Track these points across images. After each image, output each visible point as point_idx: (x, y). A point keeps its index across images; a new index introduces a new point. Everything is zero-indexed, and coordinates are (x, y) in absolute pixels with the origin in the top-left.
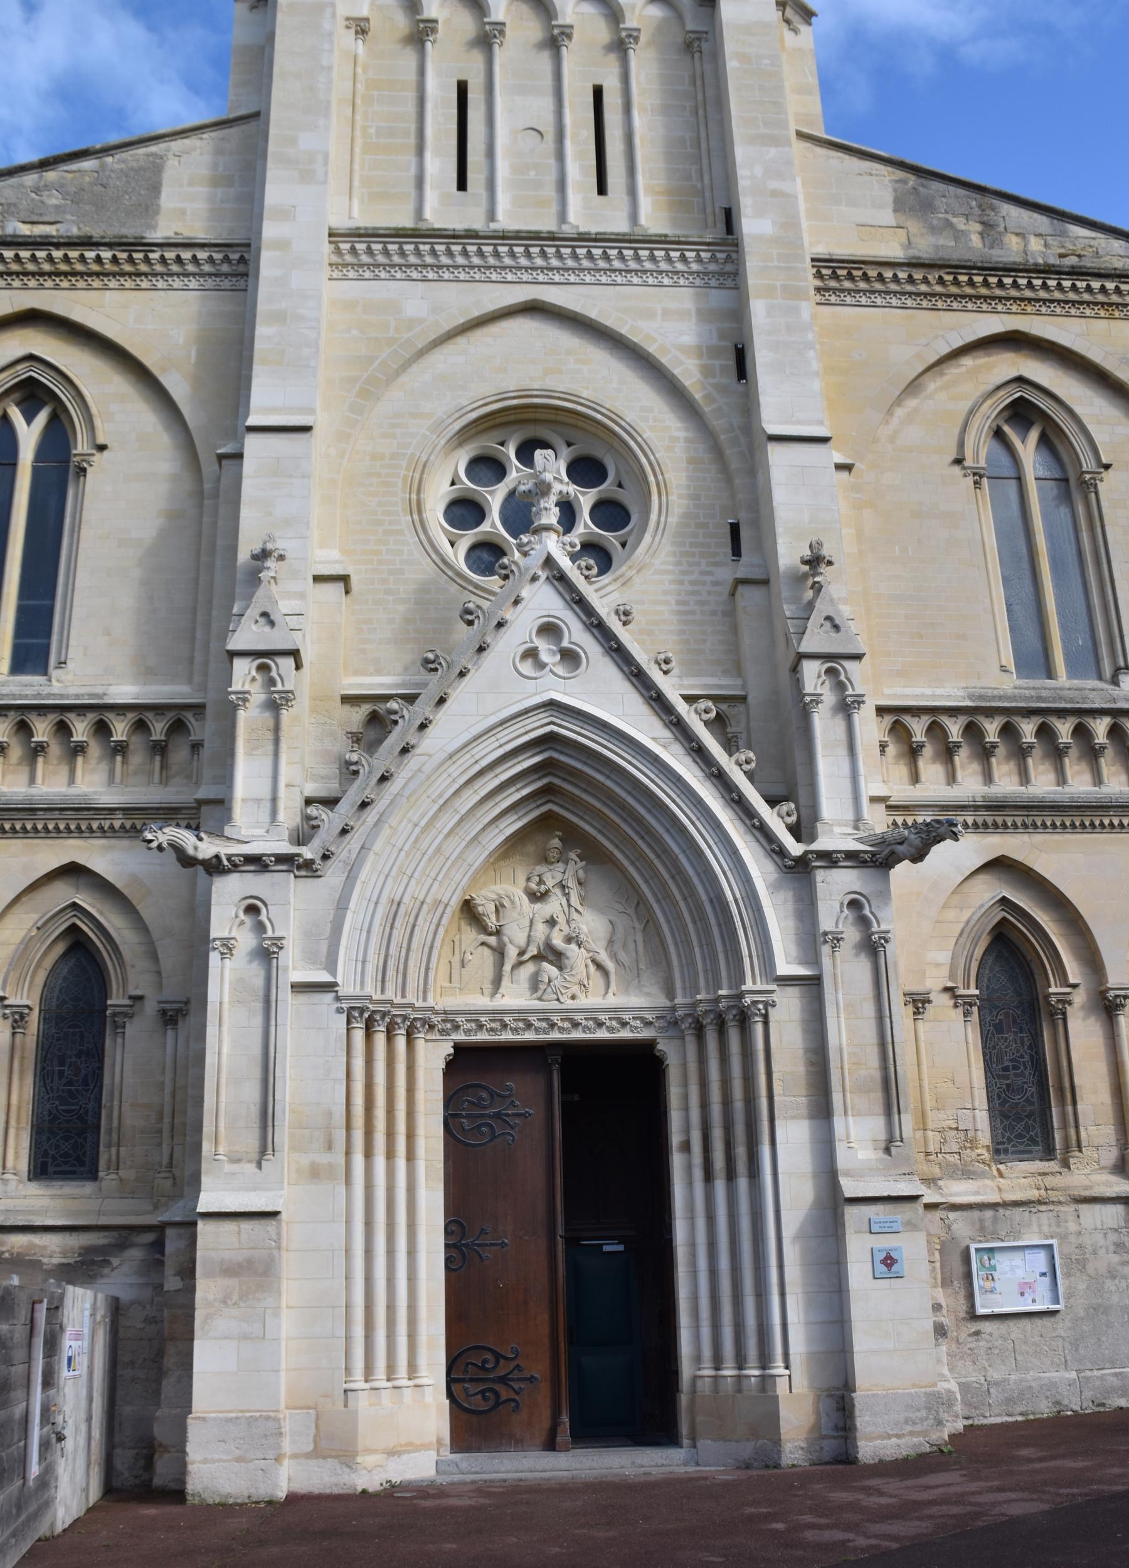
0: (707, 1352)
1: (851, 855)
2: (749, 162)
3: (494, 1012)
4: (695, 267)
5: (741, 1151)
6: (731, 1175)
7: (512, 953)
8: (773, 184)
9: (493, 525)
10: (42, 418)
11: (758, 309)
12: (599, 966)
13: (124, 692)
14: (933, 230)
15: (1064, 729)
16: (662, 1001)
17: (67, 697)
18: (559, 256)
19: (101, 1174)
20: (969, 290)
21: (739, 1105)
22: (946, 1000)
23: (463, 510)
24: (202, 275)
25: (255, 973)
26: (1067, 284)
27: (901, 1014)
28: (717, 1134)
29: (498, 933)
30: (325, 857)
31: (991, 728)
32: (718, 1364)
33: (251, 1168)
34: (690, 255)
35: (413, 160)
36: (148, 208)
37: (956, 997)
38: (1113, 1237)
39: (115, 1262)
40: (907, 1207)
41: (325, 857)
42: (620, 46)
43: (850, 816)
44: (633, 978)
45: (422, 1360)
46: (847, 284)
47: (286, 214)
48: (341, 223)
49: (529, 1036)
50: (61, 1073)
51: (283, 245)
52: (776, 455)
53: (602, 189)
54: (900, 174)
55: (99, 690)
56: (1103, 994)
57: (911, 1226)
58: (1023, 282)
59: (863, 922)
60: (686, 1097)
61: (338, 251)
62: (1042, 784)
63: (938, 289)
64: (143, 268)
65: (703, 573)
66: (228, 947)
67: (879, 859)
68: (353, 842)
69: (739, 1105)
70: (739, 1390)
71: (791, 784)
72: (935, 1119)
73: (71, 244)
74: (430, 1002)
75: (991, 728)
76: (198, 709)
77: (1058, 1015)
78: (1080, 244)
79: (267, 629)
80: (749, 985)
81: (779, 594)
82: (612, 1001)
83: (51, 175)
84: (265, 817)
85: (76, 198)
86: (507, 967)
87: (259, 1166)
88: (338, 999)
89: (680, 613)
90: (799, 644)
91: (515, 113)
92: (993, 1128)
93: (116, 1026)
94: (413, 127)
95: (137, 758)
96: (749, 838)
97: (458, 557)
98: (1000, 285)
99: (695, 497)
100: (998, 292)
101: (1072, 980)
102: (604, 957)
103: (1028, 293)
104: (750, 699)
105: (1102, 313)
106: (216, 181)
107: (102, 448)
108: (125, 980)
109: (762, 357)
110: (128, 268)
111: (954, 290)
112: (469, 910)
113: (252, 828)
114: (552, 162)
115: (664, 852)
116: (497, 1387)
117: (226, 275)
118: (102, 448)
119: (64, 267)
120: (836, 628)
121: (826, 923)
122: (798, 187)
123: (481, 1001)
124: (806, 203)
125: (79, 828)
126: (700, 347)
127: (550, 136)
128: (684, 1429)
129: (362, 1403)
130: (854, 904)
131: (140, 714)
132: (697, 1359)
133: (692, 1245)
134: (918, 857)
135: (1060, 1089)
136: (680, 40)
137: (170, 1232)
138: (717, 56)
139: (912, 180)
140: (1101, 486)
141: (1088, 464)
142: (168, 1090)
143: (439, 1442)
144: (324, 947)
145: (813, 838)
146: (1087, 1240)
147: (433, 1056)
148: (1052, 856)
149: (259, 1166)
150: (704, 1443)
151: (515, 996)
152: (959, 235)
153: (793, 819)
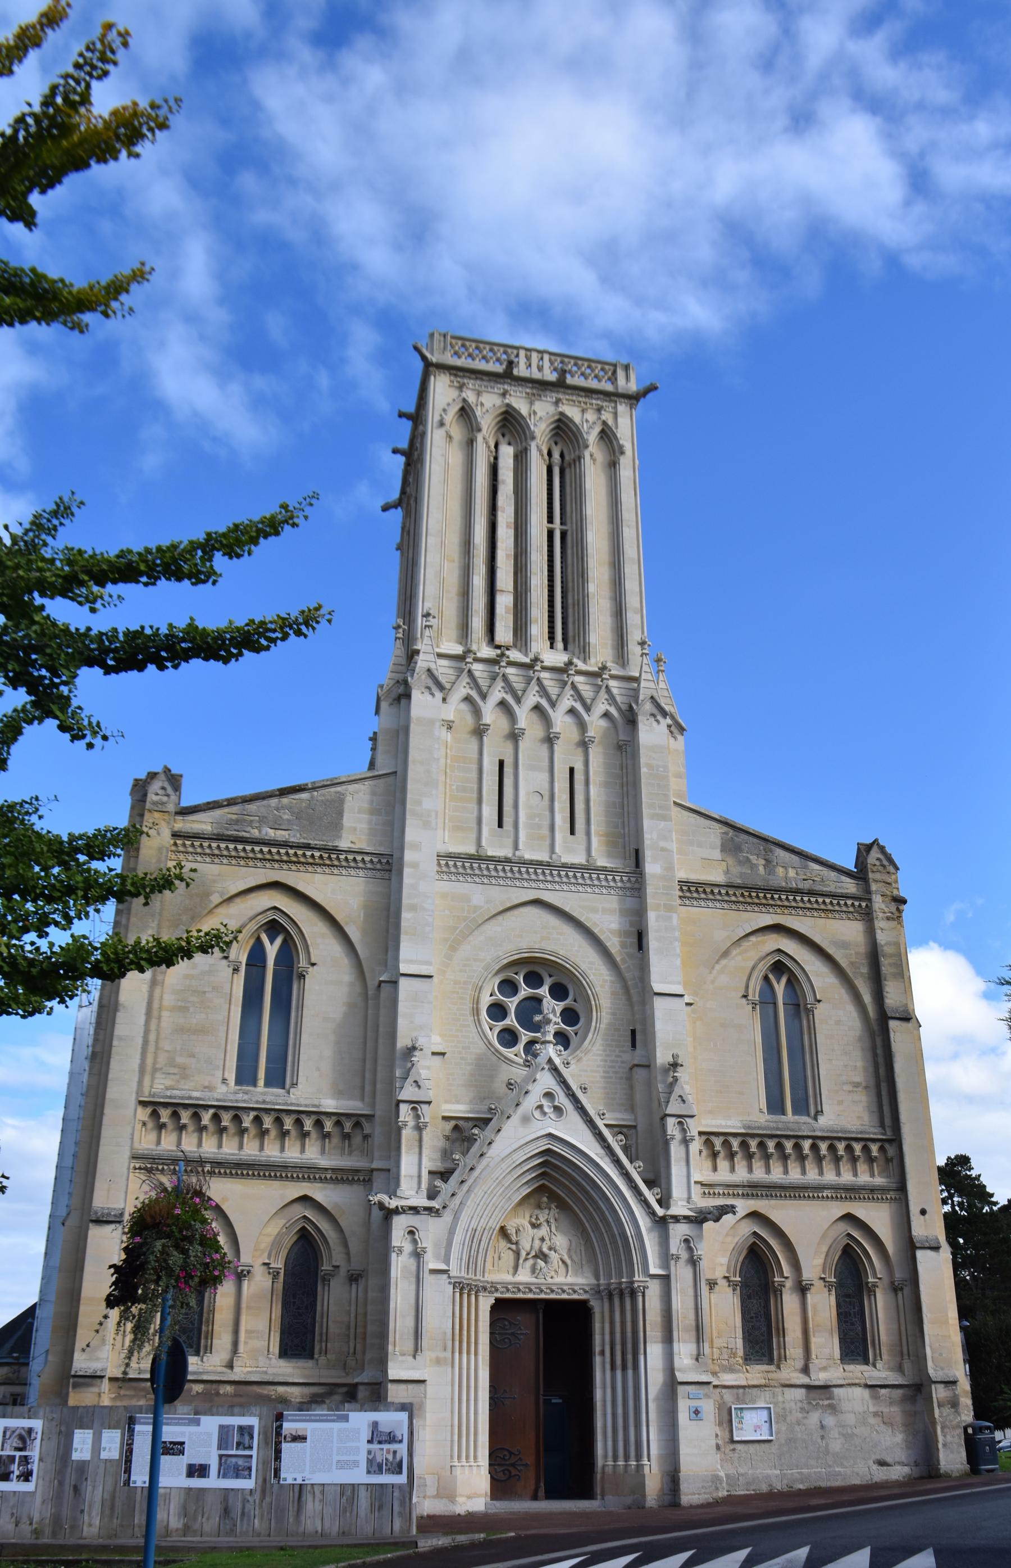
0: (610, 1454)
1: (686, 1217)
2: (652, 831)
3: (515, 1283)
4: (619, 884)
5: (630, 1357)
6: (624, 1368)
7: (523, 1254)
8: (662, 844)
9: (512, 1021)
10: (279, 941)
11: (652, 916)
12: (563, 1262)
13: (330, 1104)
14: (740, 863)
15: (789, 1145)
16: (593, 1281)
17: (301, 1106)
18: (551, 875)
19: (316, 1356)
20: (756, 901)
21: (629, 1335)
22: (725, 1283)
23: (498, 1011)
24: (366, 869)
25: (412, 1263)
26: (806, 899)
27: (704, 1288)
28: (618, 1348)
29: (517, 1243)
30: (444, 1207)
31: (753, 1144)
32: (615, 1458)
33: (411, 1358)
34: (618, 878)
35: (475, 807)
36: (336, 826)
37: (729, 1281)
38: (799, 1405)
39: (327, 1401)
40: (705, 1387)
41: (444, 1207)
42: (584, 744)
43: (685, 1196)
44: (579, 1268)
45: (479, 1454)
46: (695, 895)
47: (417, 847)
48: (444, 849)
49: (530, 1296)
50: (294, 1303)
51: (415, 865)
52: (658, 1002)
53: (572, 832)
54: (725, 829)
55: (316, 1102)
56: (800, 1282)
57: (707, 1396)
58: (784, 897)
59: (690, 1249)
60: (603, 1329)
61: (439, 865)
62: (776, 1175)
63: (741, 899)
64: (336, 863)
65: (617, 1056)
66: (400, 1250)
67: (699, 1219)
68: (457, 1200)
69: (629, 1335)
70: (626, 1471)
71: (657, 1178)
72: (718, 1342)
73: (299, 846)
74: (486, 1279)
75: (753, 1144)
76: (370, 1117)
77: (778, 1292)
78: (814, 873)
79: (417, 1089)
80: (636, 1278)
81: (656, 1077)
82: (570, 1279)
83: (285, 800)
84: (415, 1186)
85: (298, 816)
86: (521, 1261)
87: (414, 1357)
88: (449, 1277)
89: (605, 1077)
90: (667, 1106)
91: (530, 781)
92: (744, 1347)
93: (324, 1280)
94: (475, 786)
95: (336, 1140)
96: (639, 1206)
97: (493, 1037)
98: (772, 898)
99: (614, 1014)
100: (771, 902)
101: (786, 1275)
102: (566, 1258)
103: (786, 903)
104: (639, 1128)
105: (823, 915)
106: (373, 812)
107: (313, 965)
108: (331, 1257)
109: (653, 943)
110: (328, 862)
111: (749, 900)
112: (503, 1231)
113: (411, 1191)
114: (547, 813)
115: (598, 1208)
116: (510, 1468)
117: (379, 870)
118: (313, 965)
119: (294, 859)
120: (684, 1101)
121: (673, 1250)
122: (674, 847)
123: (508, 1278)
124: (679, 851)
125: (309, 1177)
126: (620, 931)
127: (546, 798)
128: (598, 1490)
129: (458, 1472)
130: (686, 1241)
131: (339, 1119)
132: (605, 1456)
133: (604, 1401)
134: (717, 1220)
135: (778, 1329)
136: (615, 742)
137: (361, 1388)
138: (635, 755)
139: (731, 833)
140: (815, 1011)
141: (810, 999)
142: (353, 1315)
143: (486, 1495)
144: (443, 1251)
145: (668, 1208)
146: (787, 1406)
147: (486, 1302)
148: (783, 1213)
149: (414, 1357)
150: (609, 1498)
151: (524, 1276)
152: (753, 867)
153: (658, 1197)
